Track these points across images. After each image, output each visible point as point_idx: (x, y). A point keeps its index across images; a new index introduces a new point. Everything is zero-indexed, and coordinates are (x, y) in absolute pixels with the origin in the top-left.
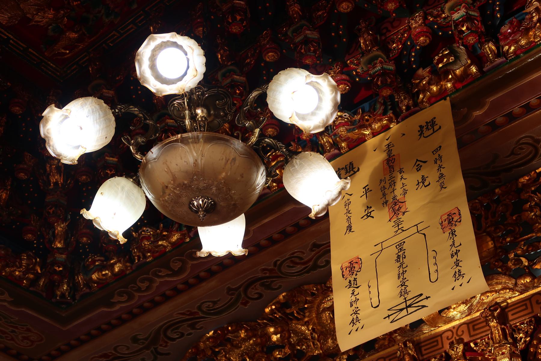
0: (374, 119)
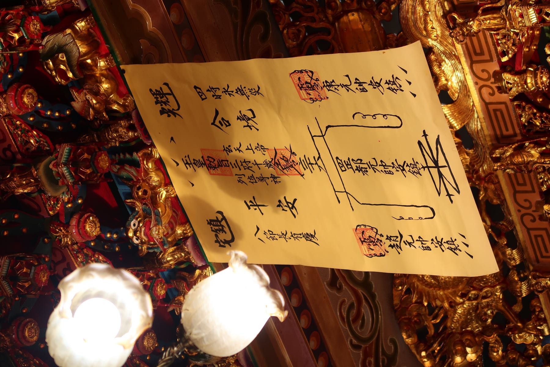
0: (144, 181)
